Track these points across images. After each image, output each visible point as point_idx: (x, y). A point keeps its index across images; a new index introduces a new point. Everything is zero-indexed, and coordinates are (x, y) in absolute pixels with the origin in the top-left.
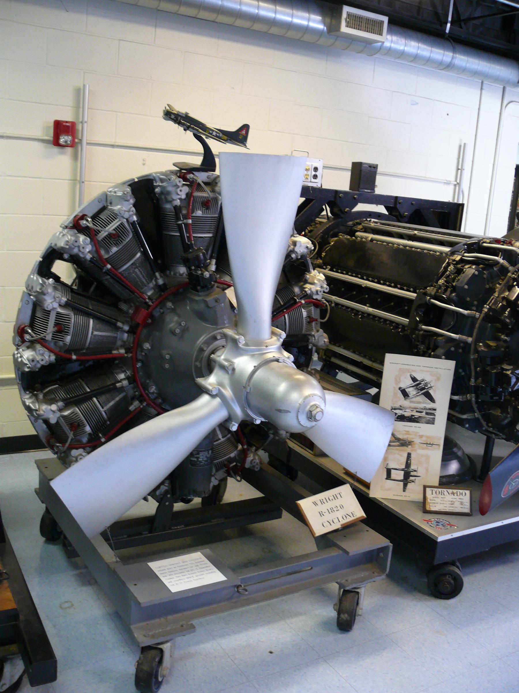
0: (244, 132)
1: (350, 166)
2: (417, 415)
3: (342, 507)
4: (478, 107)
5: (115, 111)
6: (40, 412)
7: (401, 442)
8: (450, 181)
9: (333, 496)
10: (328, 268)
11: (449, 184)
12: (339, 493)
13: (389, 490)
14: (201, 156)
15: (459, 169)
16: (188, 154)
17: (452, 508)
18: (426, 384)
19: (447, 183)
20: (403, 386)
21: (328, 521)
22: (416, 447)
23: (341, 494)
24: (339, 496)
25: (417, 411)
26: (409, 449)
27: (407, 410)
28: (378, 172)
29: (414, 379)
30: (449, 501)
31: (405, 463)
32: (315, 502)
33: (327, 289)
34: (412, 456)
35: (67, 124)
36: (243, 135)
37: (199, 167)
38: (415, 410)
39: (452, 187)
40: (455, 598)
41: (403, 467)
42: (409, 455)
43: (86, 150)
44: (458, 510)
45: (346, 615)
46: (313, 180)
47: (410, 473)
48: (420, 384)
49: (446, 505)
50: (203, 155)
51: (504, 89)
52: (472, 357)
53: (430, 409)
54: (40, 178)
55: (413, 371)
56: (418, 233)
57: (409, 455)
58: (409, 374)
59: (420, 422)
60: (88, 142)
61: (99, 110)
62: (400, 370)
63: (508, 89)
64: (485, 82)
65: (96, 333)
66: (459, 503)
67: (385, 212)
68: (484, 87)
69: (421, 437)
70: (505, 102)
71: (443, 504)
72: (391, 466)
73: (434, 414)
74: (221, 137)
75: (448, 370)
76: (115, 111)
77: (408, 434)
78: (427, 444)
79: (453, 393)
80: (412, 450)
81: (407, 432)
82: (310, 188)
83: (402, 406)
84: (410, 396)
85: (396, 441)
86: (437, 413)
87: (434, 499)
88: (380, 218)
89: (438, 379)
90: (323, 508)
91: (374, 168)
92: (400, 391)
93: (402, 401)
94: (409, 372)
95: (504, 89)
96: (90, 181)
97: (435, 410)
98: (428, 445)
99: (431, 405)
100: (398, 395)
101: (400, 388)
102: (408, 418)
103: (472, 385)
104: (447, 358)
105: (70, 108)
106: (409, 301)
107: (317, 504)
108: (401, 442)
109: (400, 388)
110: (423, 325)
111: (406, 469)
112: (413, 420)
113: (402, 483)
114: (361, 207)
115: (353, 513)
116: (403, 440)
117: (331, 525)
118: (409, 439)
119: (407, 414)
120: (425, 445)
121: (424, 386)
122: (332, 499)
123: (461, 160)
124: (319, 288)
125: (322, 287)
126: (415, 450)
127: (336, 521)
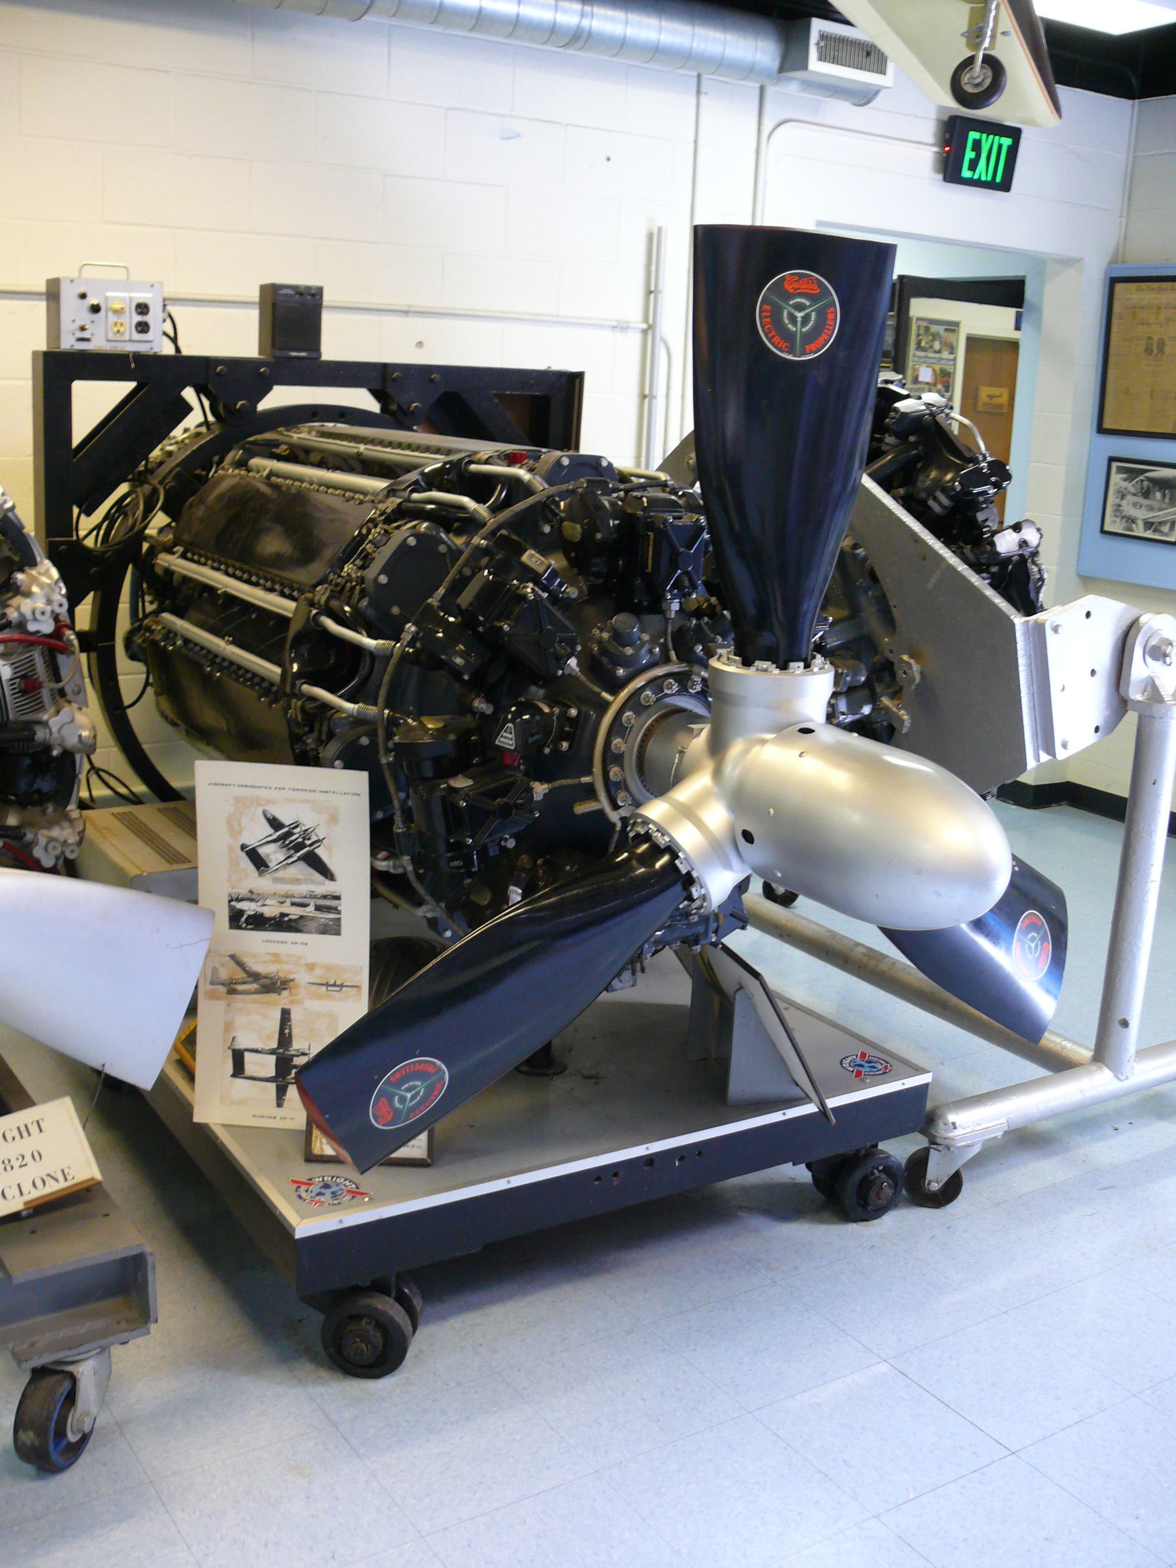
1: (255, 295)
2: (295, 912)
3: (37, 1156)
4: (692, 138)
7: (262, 981)
8: (628, 322)
10: (177, 551)
11: (626, 328)
12: (38, 1122)
13: (242, 1102)
15: (651, 292)
18: (306, 834)
19: (621, 327)
20: (252, 842)
22: (302, 993)
23: (41, 1122)
24: (34, 1129)
25: (293, 904)
26: (283, 1000)
27: (268, 902)
28: (325, 303)
29: (275, 823)
31: (277, 1036)
33: (61, 605)
34: (293, 1016)
38: (288, 901)
39: (635, 339)
40: (397, 1371)
41: (274, 1045)
42: (286, 1015)
45: (31, 1434)
46: (137, 336)
47: (292, 1060)
48: (289, 834)
51: (762, 89)
52: (384, 761)
53: (325, 897)
55: (269, 802)
56: (366, 449)
57: (286, 1015)
58: (260, 814)
59: (305, 930)
62: (238, 800)
63: (770, 91)
64: (705, 77)
67: (373, 406)
68: (703, 89)
69: (311, 967)
70: (768, 125)
72: (241, 1044)
73: (335, 910)
75: (354, 794)
77: (279, 962)
78: (327, 985)
79: (374, 852)
80: (291, 1003)
81: (276, 957)
82: (131, 356)
83: (256, 892)
84: (270, 865)
85: (249, 979)
86: (343, 906)
88: (316, 419)
89: (334, 819)
91: (313, 295)
92: (243, 855)
93: (253, 880)
94: (259, 805)
95: (762, 89)
97: (338, 898)
98: (330, 988)
99: (326, 887)
101: (243, 847)
102: (273, 922)
103: (398, 833)
104: (348, 766)
106: (283, 622)
108: (262, 981)
109: (243, 847)
110: (304, 683)
111: (281, 1051)
112: (285, 925)
113: (272, 1087)
114: (280, 397)
115: (66, 1171)
116: (265, 977)
118: (281, 975)
119: (271, 910)
120: (324, 988)
121: (300, 840)
122: (14, 1139)
123: (653, 268)
124: (40, 604)
125: (49, 601)
126: (299, 1002)
127: (12, 1192)
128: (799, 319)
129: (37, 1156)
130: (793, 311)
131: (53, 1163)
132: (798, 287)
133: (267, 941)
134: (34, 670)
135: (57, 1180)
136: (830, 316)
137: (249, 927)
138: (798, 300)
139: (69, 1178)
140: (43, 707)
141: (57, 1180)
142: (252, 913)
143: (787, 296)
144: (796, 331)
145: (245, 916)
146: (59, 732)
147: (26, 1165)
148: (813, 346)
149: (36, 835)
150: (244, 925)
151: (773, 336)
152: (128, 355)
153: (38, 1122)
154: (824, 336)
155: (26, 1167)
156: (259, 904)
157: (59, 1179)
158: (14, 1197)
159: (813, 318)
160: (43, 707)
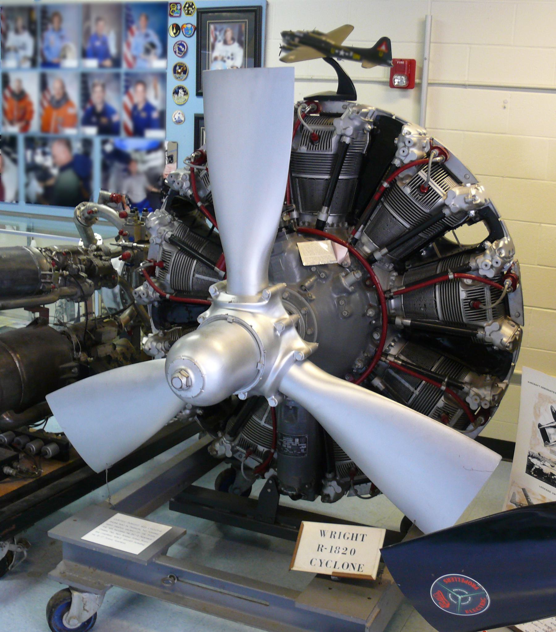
0: (383, 48)
5: (469, 44)
6: (145, 346)
9: (353, 534)
12: (363, 535)
16: (500, 88)
20: (544, 424)
21: (321, 560)
23: (365, 536)
24: (360, 538)
27: (546, 463)
30: (546, 625)
32: (324, 531)
35: (401, 62)
37: (335, 94)
43: (428, 92)
60: (429, 82)
61: (448, 43)
65: (197, 276)
76: (469, 44)
84: (550, 441)
90: (327, 542)
93: (540, 448)
94: (550, 402)
100: (538, 436)
101: (540, 425)
102: (546, 476)
107: (324, 535)
109: (540, 425)
112: (551, 481)
117: (321, 566)
122: (348, 538)
127: (331, 564)
129: (354, 552)
131: (355, 560)
133: (541, 487)
134: (483, 297)
135: (354, 568)
137: (535, 475)
139: (360, 570)
140: (486, 319)
141: (354, 568)
142: (538, 467)
145: (534, 468)
146: (490, 335)
147: (345, 554)
148: (473, 586)
149: (470, 389)
150: (533, 473)
152: (248, 67)
153: (363, 535)
155: (344, 555)
156: (542, 463)
157: (355, 569)
158: (330, 567)
160: (486, 319)
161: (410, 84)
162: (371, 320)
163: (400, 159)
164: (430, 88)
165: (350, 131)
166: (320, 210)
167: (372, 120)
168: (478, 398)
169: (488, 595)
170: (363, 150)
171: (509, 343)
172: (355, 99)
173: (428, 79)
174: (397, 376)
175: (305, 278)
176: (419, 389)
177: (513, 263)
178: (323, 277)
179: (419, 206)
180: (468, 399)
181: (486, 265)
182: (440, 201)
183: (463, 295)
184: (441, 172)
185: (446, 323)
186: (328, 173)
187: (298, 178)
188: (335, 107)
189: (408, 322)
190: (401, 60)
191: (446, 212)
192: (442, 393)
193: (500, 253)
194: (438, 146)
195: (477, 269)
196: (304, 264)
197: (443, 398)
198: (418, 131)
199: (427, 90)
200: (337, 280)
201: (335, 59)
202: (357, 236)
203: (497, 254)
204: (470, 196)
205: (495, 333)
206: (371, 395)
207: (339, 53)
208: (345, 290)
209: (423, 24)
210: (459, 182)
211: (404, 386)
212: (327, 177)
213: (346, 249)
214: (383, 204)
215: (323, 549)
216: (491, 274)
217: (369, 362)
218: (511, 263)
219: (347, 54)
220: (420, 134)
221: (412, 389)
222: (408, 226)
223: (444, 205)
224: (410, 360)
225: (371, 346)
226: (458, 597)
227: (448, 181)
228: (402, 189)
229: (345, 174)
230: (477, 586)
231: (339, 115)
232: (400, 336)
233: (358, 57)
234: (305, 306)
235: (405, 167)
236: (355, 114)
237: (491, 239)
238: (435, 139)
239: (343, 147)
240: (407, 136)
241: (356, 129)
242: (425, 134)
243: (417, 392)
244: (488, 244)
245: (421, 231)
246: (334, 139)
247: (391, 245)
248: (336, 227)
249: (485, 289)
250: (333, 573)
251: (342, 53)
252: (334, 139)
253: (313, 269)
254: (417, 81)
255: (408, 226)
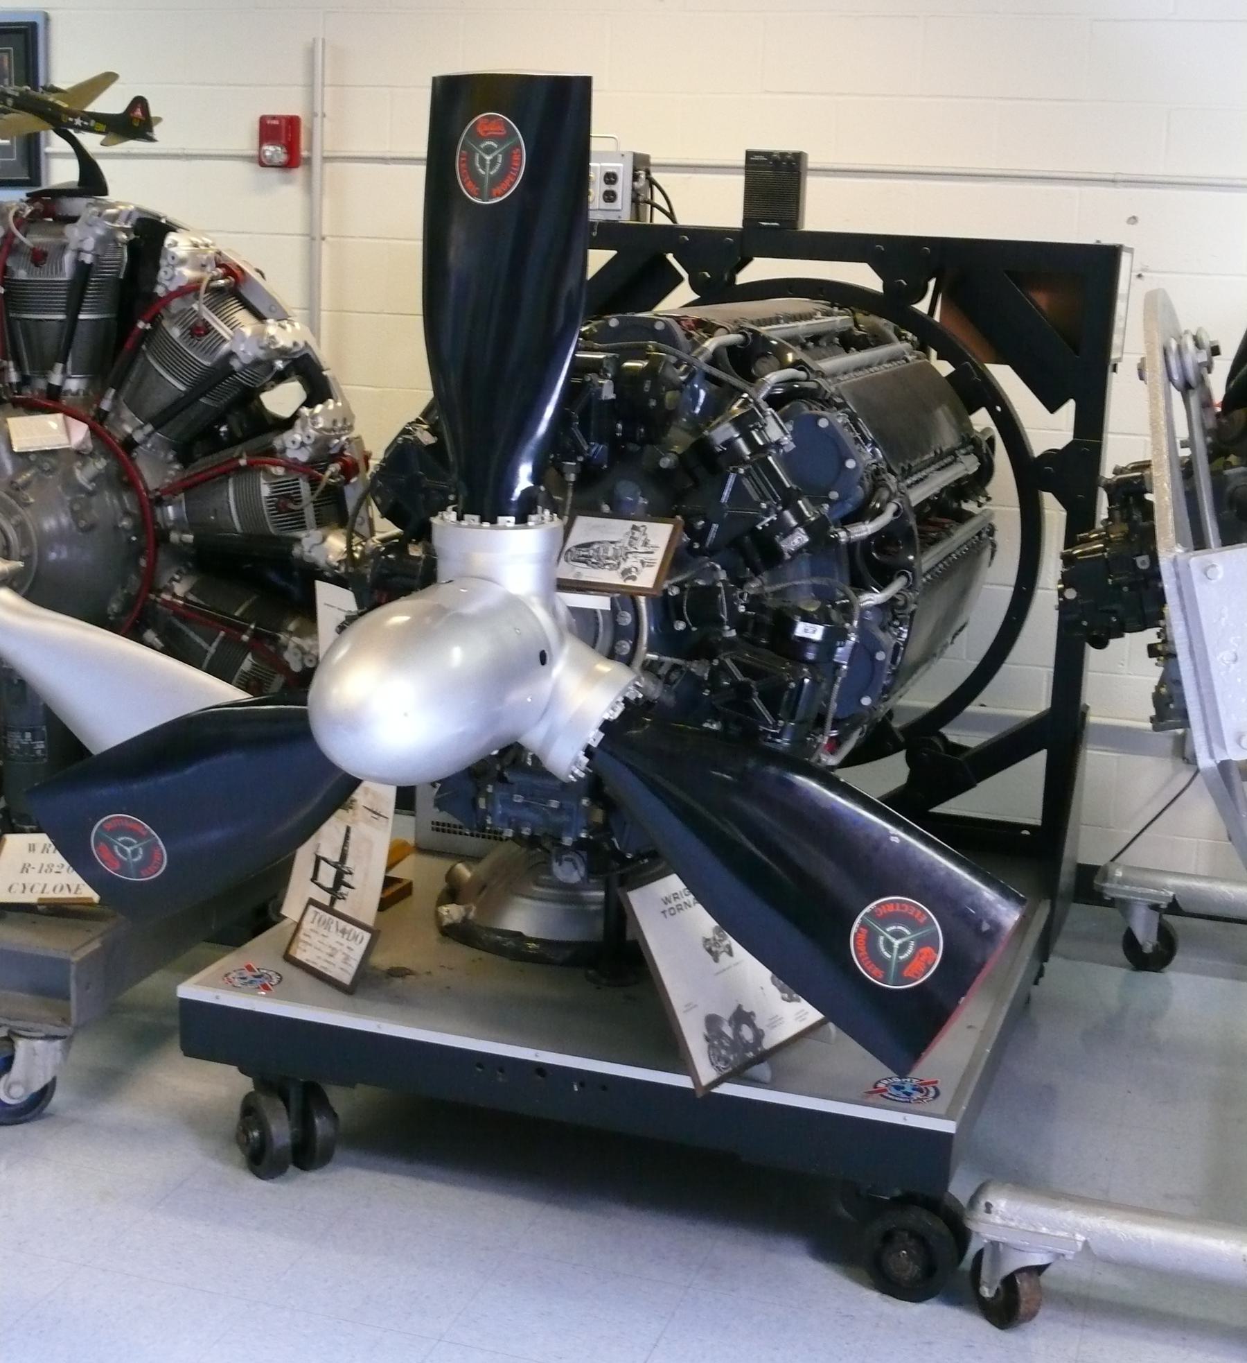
14: (738, 174)
17: (325, 965)
30: (330, 947)
36: (140, 120)
37: (76, 187)
43: (327, 173)
44: (333, 972)
49: (320, 954)
50: (425, 162)
54: (247, 233)
60: (325, 154)
66: (343, 956)
71: (319, 950)
74: (94, 127)
87: (312, 934)
96: (343, 237)
105: (300, 88)
114: (760, 269)
117: (23, 892)
120: (370, 814)
127: (38, 889)
128: (893, 940)
130: (904, 939)
132: (922, 959)
136: (516, 158)
138: (488, 143)
139: (79, 892)
143: (921, 943)
144: (500, 153)
149: (289, 639)
151: (895, 907)
154: (864, 953)
159: (885, 953)
160: (305, 526)
161: (293, 160)
162: (129, 535)
163: (163, 285)
164: (329, 167)
165: (89, 244)
166: (51, 368)
167: (128, 226)
168: (299, 652)
169: (160, 843)
170: (118, 273)
171: (339, 562)
172: (104, 191)
173: (322, 151)
174: (184, 627)
175: (19, 470)
176: (215, 644)
177: (347, 439)
178: (46, 469)
179: (192, 354)
180: (287, 656)
181: (294, 442)
182: (225, 347)
183: (266, 491)
184: (233, 303)
185: (248, 537)
186: (62, 311)
187: (19, 319)
188: (77, 205)
189: (189, 538)
190: (274, 118)
191: (236, 364)
192: (247, 648)
193: (314, 424)
194: (227, 263)
195: (284, 450)
196: (16, 450)
197: (249, 657)
198: (192, 242)
199: (322, 169)
200: (68, 476)
201: (71, 131)
202: (106, 405)
203: (310, 424)
204: (265, 338)
205: (316, 547)
206: (91, 630)
207: (74, 122)
208: (81, 489)
209: (311, 52)
210: (260, 317)
211: (195, 642)
212: (61, 317)
213: (84, 427)
214: (145, 356)
215: (30, 869)
216: (303, 456)
217: (129, 604)
218: (344, 438)
219: (86, 123)
220: (196, 245)
221: (204, 645)
222: (182, 388)
223: (231, 354)
224: (202, 600)
225: (134, 577)
226: (126, 850)
227: (242, 316)
228: (168, 330)
229: (91, 312)
230: (859, 931)
231: (74, 220)
232: (190, 565)
233: (102, 127)
234: (16, 512)
235: (171, 295)
236: (95, 218)
237: (309, 403)
238: (224, 252)
239: (83, 271)
240: (172, 249)
241: (101, 241)
242: (207, 245)
243: (212, 650)
244: (306, 411)
245: (203, 395)
246: (68, 258)
247: (159, 421)
248: (84, 395)
249: (301, 481)
250: (40, 899)
251: (78, 122)
252: (68, 258)
253: (32, 458)
254: (304, 153)
255: (182, 388)
